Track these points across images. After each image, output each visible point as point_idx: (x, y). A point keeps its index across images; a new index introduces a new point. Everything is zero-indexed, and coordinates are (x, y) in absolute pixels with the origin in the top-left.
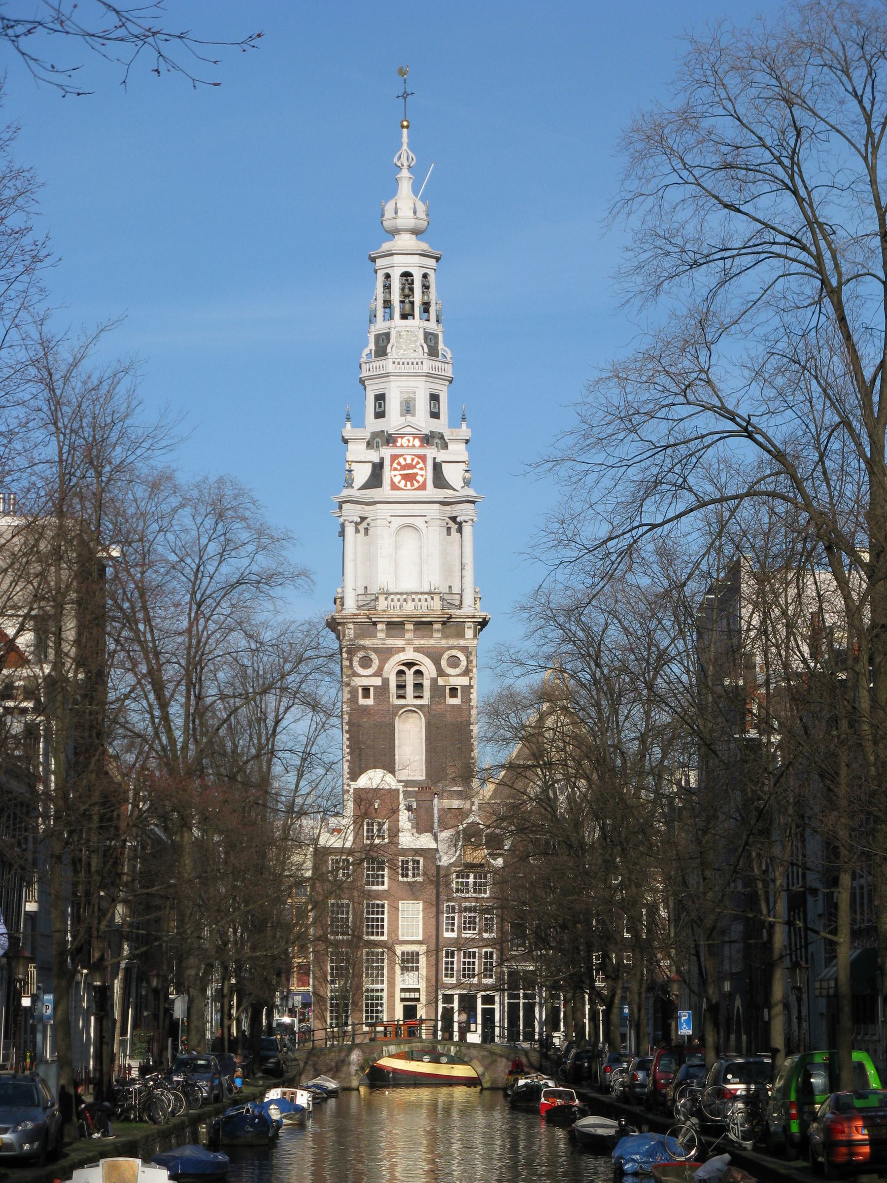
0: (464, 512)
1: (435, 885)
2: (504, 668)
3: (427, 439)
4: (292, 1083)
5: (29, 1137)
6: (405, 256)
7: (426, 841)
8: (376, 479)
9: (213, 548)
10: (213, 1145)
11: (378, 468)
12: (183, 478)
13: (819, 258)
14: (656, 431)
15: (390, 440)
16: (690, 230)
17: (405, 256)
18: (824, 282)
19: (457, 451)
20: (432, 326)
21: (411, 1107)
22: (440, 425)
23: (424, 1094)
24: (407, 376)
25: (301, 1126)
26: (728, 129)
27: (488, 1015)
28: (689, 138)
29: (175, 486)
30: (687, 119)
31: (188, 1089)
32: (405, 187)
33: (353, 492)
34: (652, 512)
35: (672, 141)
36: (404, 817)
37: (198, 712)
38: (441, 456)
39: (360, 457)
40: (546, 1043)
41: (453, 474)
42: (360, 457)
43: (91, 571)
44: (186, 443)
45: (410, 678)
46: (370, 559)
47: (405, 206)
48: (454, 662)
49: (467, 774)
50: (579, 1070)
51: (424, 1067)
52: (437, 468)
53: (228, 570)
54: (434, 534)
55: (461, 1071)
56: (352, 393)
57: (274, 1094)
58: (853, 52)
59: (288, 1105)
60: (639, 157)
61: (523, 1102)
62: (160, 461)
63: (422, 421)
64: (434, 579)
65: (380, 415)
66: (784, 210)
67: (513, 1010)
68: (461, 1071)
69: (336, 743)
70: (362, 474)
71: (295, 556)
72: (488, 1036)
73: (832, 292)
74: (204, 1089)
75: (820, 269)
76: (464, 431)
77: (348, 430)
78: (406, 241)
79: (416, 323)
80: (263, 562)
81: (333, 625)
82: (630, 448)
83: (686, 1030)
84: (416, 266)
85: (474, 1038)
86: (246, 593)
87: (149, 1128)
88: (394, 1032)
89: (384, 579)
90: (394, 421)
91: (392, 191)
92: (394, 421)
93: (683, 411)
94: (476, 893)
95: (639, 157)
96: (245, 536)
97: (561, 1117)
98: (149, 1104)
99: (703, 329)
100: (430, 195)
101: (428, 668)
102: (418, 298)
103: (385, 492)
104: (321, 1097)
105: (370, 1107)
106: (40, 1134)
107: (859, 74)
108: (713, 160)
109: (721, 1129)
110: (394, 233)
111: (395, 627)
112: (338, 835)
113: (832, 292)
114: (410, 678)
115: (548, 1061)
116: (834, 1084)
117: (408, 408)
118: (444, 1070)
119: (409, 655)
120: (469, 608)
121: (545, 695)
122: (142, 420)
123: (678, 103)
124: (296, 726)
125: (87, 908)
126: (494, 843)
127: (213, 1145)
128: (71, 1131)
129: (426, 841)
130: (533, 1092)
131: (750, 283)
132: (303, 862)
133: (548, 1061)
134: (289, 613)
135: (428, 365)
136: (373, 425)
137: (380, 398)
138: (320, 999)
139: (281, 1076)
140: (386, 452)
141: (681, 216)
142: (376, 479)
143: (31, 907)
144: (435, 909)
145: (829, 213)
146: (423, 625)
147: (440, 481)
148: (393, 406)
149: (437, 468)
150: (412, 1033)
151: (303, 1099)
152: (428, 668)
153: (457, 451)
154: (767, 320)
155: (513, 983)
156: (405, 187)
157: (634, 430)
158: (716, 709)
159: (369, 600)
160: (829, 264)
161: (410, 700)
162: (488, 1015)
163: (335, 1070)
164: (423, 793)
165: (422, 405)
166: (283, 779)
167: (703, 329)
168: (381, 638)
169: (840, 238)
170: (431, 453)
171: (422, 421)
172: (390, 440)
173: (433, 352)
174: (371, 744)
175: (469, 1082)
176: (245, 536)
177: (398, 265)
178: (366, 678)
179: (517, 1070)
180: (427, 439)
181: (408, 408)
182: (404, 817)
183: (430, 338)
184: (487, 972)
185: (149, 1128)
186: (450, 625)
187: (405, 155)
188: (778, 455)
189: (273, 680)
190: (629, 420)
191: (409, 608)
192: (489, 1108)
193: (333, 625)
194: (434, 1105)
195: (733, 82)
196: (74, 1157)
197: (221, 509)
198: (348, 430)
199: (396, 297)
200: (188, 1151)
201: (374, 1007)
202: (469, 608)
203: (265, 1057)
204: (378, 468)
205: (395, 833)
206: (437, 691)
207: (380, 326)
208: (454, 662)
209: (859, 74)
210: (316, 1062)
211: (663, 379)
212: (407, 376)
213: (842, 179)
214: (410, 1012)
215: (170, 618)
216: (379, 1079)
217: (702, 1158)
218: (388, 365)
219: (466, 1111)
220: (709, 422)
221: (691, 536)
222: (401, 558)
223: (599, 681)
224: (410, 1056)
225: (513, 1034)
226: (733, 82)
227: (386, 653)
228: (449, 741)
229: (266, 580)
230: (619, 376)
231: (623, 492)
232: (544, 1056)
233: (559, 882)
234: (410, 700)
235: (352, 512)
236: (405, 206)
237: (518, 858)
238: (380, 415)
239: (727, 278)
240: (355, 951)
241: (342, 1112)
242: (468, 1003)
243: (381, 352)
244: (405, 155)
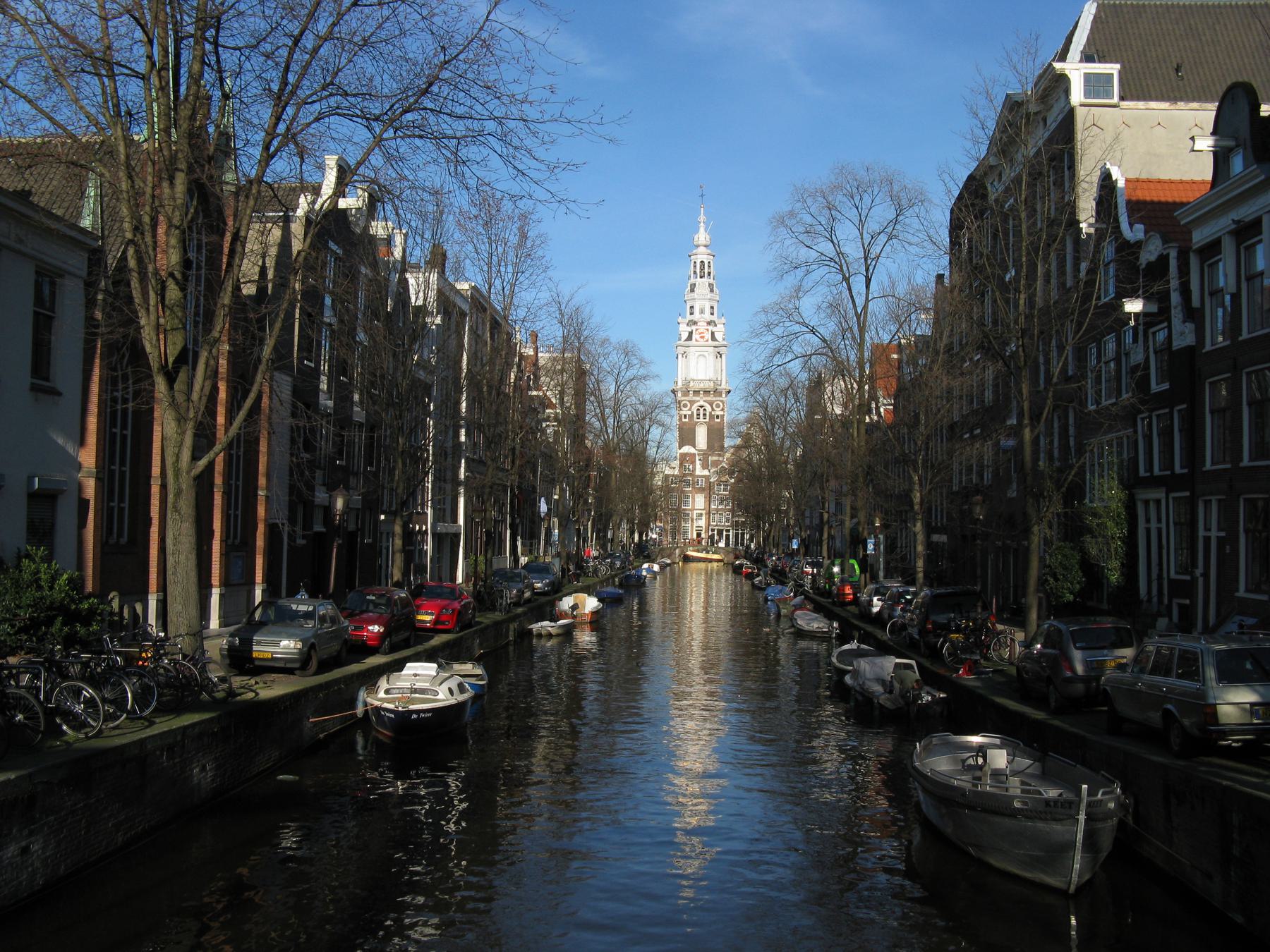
0: (723, 350)
1: (709, 490)
2: (733, 410)
3: (709, 323)
4: (653, 561)
5: (547, 585)
6: (702, 255)
7: (706, 472)
8: (690, 337)
9: (624, 366)
10: (621, 586)
11: (691, 333)
12: (613, 340)
13: (841, 266)
14: (779, 331)
15: (695, 323)
16: (794, 255)
17: (702, 255)
18: (844, 275)
19: (720, 327)
20: (711, 281)
21: (699, 572)
22: (714, 318)
23: (702, 565)
24: (702, 299)
25: (655, 578)
26: (809, 219)
27: (728, 537)
28: (794, 221)
29: (1011, 110)
30: (792, 214)
31: (612, 565)
32: (702, 230)
33: (681, 342)
34: (777, 360)
35: (788, 222)
36: (698, 463)
37: (619, 426)
38: (714, 329)
39: (684, 330)
40: (748, 547)
41: (719, 336)
42: (684, 330)
43: (581, 374)
44: (612, 326)
45: (701, 412)
46: (687, 367)
47: (702, 237)
48: (718, 406)
49: (722, 448)
50: (758, 561)
51: (703, 555)
52: (713, 333)
53: (629, 374)
54: (711, 358)
55: (716, 557)
56: (679, 305)
57: (646, 566)
58: (855, 190)
59: (649, 570)
60: (775, 228)
61: (737, 570)
62: (602, 335)
63: (707, 316)
64: (711, 375)
65: (692, 314)
66: (828, 249)
67: (737, 535)
68: (716, 557)
69: (673, 437)
70: (685, 335)
71: (654, 369)
72: (727, 544)
73: (846, 279)
74: (618, 564)
75: (841, 270)
76: (723, 320)
77: (680, 320)
78: (702, 249)
79: (705, 279)
80: (642, 372)
81: (674, 392)
82: (770, 338)
83: (795, 547)
84: (706, 259)
85: (722, 545)
86: (634, 383)
87: (596, 580)
88: (691, 543)
89: (693, 375)
90: (697, 316)
91: (697, 231)
92: (697, 316)
93: (787, 324)
94: (722, 491)
95: (775, 228)
96: (636, 362)
97: (750, 576)
98: (596, 571)
99: (798, 292)
100: (711, 232)
101: (709, 408)
102: (706, 270)
103: (693, 342)
104: (662, 568)
105: (683, 571)
106: (551, 584)
107: (857, 199)
108: (802, 229)
109: (802, 586)
110: (698, 246)
111: (696, 392)
112: (672, 470)
113: (846, 279)
114: (701, 412)
115: (747, 555)
116: (842, 571)
117: (702, 312)
118: (710, 556)
119: (702, 403)
120: (724, 386)
121: (747, 421)
122: (595, 321)
123: (790, 208)
124: (655, 433)
125: (579, 496)
126: (731, 474)
127: (621, 586)
128: (565, 581)
129: (706, 472)
130: (741, 566)
131: (815, 276)
132: (658, 481)
133: (747, 555)
134: (653, 389)
135: (710, 295)
136: (689, 317)
137: (692, 307)
138: (666, 530)
139: (650, 559)
140: (694, 328)
141: (791, 249)
142: (690, 337)
143: (556, 497)
144: (709, 500)
145: (845, 250)
146: (707, 392)
147: (713, 338)
148: (697, 310)
149: (713, 333)
150: (699, 542)
151: (656, 568)
152: (709, 408)
153: (720, 327)
154: (822, 289)
155: (736, 525)
156: (702, 230)
157: (770, 330)
158: (809, 431)
159: (687, 384)
160: (845, 269)
161: (701, 419)
162: (728, 537)
163: (669, 557)
164: (705, 455)
165: (708, 310)
166: (651, 451)
167: (798, 292)
168: (691, 397)
169: (850, 260)
170: (710, 328)
171: (707, 316)
172: (695, 323)
173: (712, 291)
174: (687, 436)
175: (718, 561)
176: (636, 362)
177: (699, 259)
178: (685, 411)
179: (737, 558)
180: (709, 323)
181: (702, 312)
182: (698, 463)
183: (711, 285)
184: (728, 520)
185: (596, 580)
186: (717, 392)
187: (702, 218)
188: (824, 341)
189: (648, 414)
190: (769, 327)
191: (702, 385)
192: (727, 573)
193: (674, 392)
194: (707, 571)
195: (809, 201)
196: (565, 591)
197: (627, 352)
198: (680, 320)
199: (698, 270)
200: (610, 589)
201: (686, 533)
202: (724, 386)
203: (644, 552)
204: (691, 333)
205: (694, 469)
206: (711, 416)
207: (692, 280)
208: (718, 406)
209: (857, 199)
210: (663, 552)
211: (781, 312)
212: (702, 299)
213: (851, 237)
214: (699, 535)
215: (609, 389)
216: (687, 559)
217: (795, 596)
218: (695, 295)
219: (718, 573)
220: (797, 328)
221: (795, 367)
222: (700, 366)
223: (767, 418)
224: (698, 551)
225: (737, 543)
226: (809, 201)
227: (692, 402)
228: (716, 435)
229: (645, 378)
230: (765, 311)
231: (768, 352)
232: (746, 552)
233: (756, 487)
234: (701, 419)
235: (681, 350)
236: (702, 237)
237: (739, 481)
238: (692, 314)
239: (808, 272)
240: (678, 515)
241: (672, 573)
242: (720, 533)
243: (692, 290)
244: (702, 218)
